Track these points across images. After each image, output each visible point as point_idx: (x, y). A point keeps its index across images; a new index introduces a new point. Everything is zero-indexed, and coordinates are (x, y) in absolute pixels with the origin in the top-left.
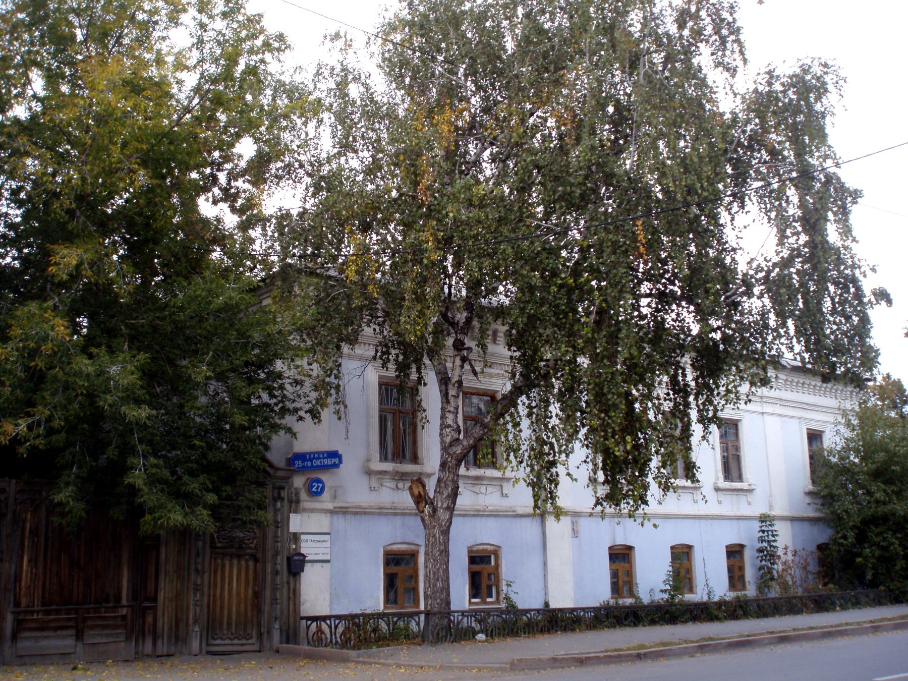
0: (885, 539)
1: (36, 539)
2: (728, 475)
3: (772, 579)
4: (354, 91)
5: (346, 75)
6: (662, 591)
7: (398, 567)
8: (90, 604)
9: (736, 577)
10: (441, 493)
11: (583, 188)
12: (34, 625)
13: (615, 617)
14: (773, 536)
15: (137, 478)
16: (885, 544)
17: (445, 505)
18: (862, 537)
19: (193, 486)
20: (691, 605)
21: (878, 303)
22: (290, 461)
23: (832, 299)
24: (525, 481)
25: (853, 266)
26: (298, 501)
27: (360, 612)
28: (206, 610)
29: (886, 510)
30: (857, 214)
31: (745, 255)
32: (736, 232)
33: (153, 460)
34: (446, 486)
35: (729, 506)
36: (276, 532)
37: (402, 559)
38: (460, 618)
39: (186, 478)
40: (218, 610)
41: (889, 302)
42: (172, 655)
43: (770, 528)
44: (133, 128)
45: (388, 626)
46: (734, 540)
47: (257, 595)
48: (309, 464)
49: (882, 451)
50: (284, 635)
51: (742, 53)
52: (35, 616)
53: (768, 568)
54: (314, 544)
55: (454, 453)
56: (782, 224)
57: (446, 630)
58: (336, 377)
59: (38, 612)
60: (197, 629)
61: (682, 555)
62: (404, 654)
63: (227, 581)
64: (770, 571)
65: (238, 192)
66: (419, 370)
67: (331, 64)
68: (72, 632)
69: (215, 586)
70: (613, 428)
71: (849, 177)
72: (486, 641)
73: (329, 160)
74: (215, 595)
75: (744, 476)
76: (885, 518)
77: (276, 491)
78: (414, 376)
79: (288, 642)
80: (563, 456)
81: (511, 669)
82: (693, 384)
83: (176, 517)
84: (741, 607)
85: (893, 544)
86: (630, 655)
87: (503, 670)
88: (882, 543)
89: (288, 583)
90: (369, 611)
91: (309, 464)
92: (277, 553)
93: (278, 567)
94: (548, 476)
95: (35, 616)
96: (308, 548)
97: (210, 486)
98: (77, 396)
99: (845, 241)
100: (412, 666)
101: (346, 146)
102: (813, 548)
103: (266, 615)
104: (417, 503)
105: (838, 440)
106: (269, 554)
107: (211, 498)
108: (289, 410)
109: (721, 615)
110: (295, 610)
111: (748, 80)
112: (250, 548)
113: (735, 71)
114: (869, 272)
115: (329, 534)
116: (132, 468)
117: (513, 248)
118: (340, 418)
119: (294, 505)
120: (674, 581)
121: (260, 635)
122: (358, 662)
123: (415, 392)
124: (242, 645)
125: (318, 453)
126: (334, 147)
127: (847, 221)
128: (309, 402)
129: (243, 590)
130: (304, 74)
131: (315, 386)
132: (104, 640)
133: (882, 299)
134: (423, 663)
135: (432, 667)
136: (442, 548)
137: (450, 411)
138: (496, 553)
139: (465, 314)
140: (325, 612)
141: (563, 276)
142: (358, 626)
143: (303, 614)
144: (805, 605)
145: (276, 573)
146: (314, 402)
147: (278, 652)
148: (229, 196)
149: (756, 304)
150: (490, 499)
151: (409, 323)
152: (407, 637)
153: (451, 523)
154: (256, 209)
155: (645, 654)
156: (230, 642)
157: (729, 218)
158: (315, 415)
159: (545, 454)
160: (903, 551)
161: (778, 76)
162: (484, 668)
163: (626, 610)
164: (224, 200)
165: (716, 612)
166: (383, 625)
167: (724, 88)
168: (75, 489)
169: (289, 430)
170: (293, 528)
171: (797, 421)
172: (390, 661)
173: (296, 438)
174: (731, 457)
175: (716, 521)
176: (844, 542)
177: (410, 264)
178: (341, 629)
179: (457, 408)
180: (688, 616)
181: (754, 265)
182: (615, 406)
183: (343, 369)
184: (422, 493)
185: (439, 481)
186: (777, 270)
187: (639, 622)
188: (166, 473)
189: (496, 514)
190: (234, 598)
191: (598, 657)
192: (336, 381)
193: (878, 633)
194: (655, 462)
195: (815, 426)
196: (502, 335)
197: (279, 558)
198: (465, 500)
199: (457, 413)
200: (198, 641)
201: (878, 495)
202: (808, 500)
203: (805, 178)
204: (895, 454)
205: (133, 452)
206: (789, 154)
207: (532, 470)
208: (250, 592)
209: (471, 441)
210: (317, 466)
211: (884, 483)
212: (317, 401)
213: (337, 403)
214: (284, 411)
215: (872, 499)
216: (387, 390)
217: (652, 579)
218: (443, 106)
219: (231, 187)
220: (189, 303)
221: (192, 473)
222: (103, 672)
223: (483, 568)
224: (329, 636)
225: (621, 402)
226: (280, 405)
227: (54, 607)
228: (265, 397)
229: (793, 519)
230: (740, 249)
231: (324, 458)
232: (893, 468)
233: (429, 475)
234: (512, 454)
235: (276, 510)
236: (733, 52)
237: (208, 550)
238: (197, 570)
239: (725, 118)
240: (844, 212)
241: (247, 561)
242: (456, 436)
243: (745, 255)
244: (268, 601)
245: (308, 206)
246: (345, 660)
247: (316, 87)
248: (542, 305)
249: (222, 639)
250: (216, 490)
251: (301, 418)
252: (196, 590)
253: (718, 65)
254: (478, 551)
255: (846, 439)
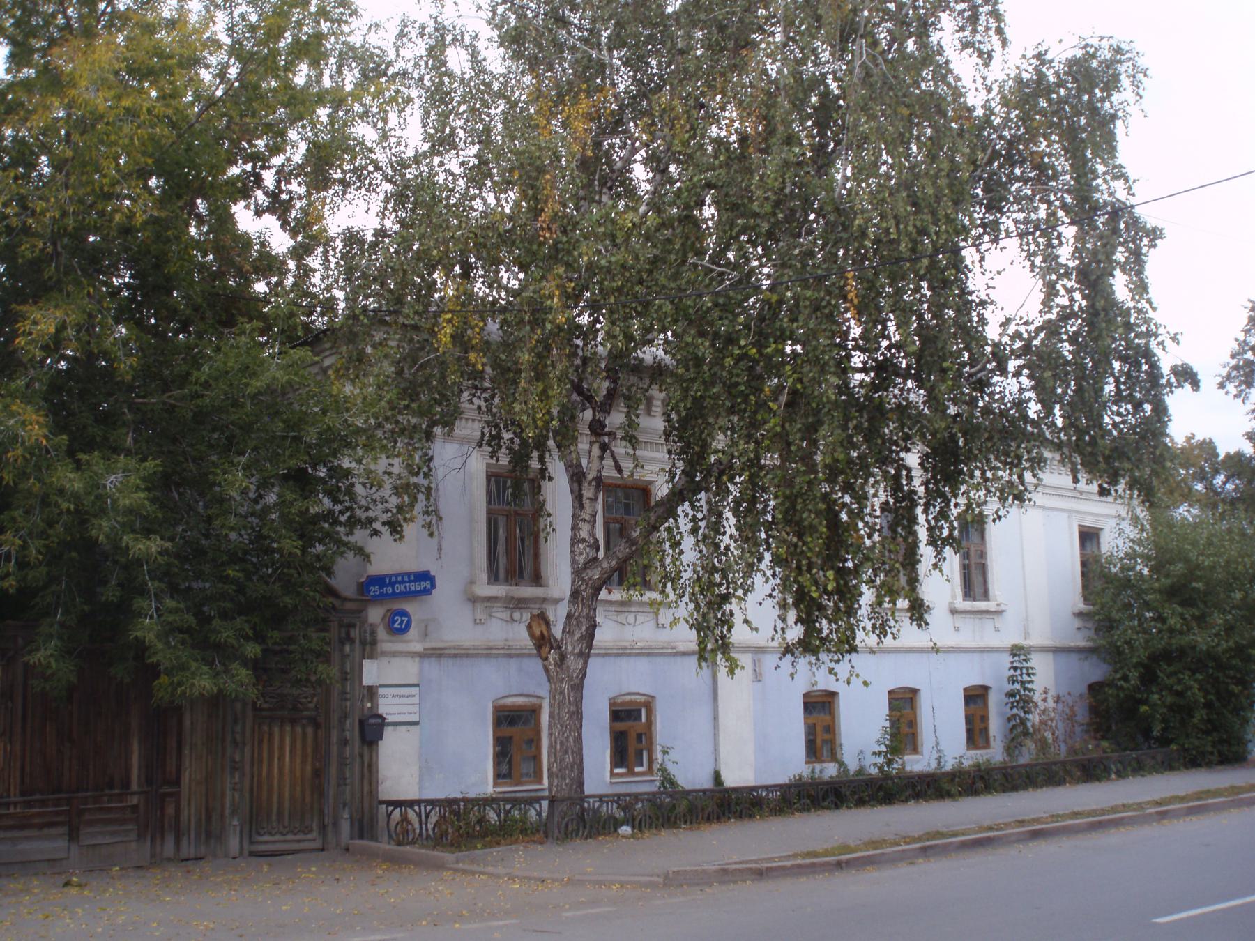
0: (1180, 681)
1: (10, 704)
2: (968, 592)
3: (1026, 734)
4: (457, 60)
5: (442, 36)
6: (875, 753)
7: (513, 728)
8: (87, 790)
9: (976, 733)
10: (571, 633)
11: (772, 220)
12: (11, 822)
13: (809, 796)
14: (1028, 675)
15: (147, 628)
16: (1179, 688)
17: (577, 650)
18: (1149, 677)
19: (225, 633)
20: (913, 777)
21: (1179, 386)
22: (363, 588)
23: (1117, 382)
24: (687, 622)
25: (1149, 334)
26: (374, 643)
27: (460, 796)
28: (247, 795)
29: (1183, 643)
30: (1156, 263)
31: (998, 312)
32: (986, 279)
33: (170, 603)
34: (578, 624)
35: (969, 634)
36: (344, 686)
37: (520, 717)
38: (597, 805)
39: (216, 623)
40: (265, 794)
41: (1195, 384)
42: (201, 858)
43: (1025, 664)
44: (132, 139)
45: (499, 815)
46: (976, 680)
47: (317, 774)
48: (390, 590)
49: (1180, 560)
50: (357, 825)
51: (999, 31)
52: (12, 810)
53: (1020, 718)
54: (397, 700)
55: (590, 579)
56: (1050, 267)
57: (580, 820)
58: (426, 476)
59: (15, 804)
60: (235, 822)
61: (903, 703)
62: (520, 860)
63: (276, 755)
64: (1023, 722)
65: (291, 199)
66: (542, 459)
67: (421, 21)
68: (63, 830)
69: (261, 761)
70: (809, 558)
71: (1149, 215)
72: (633, 836)
73: (416, 160)
74: (260, 775)
75: (991, 593)
76: (1182, 652)
77: (343, 631)
78: (535, 464)
79: (361, 837)
80: (740, 592)
81: (665, 884)
82: (921, 490)
83: (203, 683)
84: (982, 778)
85: (1191, 688)
86: (827, 864)
87: (653, 885)
88: (1175, 687)
89: (361, 756)
90: (471, 795)
91: (390, 590)
92: (344, 716)
93: (348, 734)
94: (719, 615)
95: (12, 810)
96: (389, 706)
97: (251, 633)
98: (61, 514)
99: (1138, 302)
100: (530, 879)
101: (442, 142)
102: (1083, 689)
103: (331, 801)
104: (539, 647)
105: (1121, 545)
106: (335, 717)
107: (252, 650)
108: (359, 520)
109: (953, 790)
110: (371, 792)
111: (1010, 63)
112: (307, 709)
113: (990, 57)
114: (1168, 343)
115: (417, 685)
116: (140, 615)
117: (672, 303)
118: (431, 535)
119: (370, 648)
120: (891, 741)
121: (323, 828)
122: (456, 870)
123: (536, 490)
124: (299, 841)
125: (403, 575)
126: (424, 140)
127: (1139, 273)
128: (387, 511)
129: (298, 767)
130: (381, 32)
131: (396, 488)
132: (108, 840)
133: (1185, 381)
134: (545, 875)
135: (557, 880)
136: (572, 708)
137: (584, 520)
138: (649, 704)
139: (606, 384)
140: (411, 793)
141: (743, 343)
142: (457, 814)
143: (382, 797)
144: (1068, 772)
145: (344, 742)
146: (395, 511)
147: (347, 850)
148: (278, 206)
149: (1011, 386)
150: (641, 630)
151: (525, 412)
152: (524, 831)
153: (585, 675)
154: (316, 229)
155: (848, 862)
156: (282, 838)
157: (977, 257)
158: (395, 528)
159: (715, 585)
160: (1205, 697)
161: (1051, 61)
162: (628, 883)
163: (825, 787)
164: (271, 210)
165: (946, 787)
166: (492, 816)
167: (974, 81)
168: (59, 644)
169: (360, 551)
170: (367, 680)
171: (1066, 515)
172: (500, 870)
173: (369, 561)
174: (973, 566)
175: (952, 656)
176: (1125, 685)
177: (528, 328)
178: (434, 818)
179: (594, 516)
180: (909, 792)
181: (1012, 329)
182: (813, 528)
183: (437, 462)
184: (545, 633)
185: (569, 616)
186: (1042, 335)
187: (842, 803)
188: (191, 620)
189: (649, 653)
190: (287, 778)
191: (783, 868)
192: (426, 483)
193: (1165, 822)
194: (867, 596)
195: (1090, 522)
196: (659, 403)
197: (348, 722)
198: (604, 635)
199: (594, 522)
200: (238, 839)
201: (1172, 622)
202: (1077, 623)
203: (1084, 208)
204: (1198, 567)
205: (143, 592)
206: (1062, 164)
207: (697, 608)
208: (309, 768)
209: (614, 563)
210: (401, 593)
211: (1182, 604)
212: (400, 508)
213: (427, 513)
214: (353, 523)
215: (1165, 627)
216: (497, 483)
217: (862, 734)
218: (577, 94)
219: (282, 191)
220: (216, 379)
221: (224, 615)
222: (105, 891)
223: (631, 729)
224: (417, 826)
225: (820, 523)
226: (348, 514)
227: (38, 797)
228: (327, 502)
229: (1056, 650)
230: (992, 303)
231: (410, 581)
232: (1194, 584)
233: (557, 601)
234: (669, 584)
235: (344, 657)
236: (987, 29)
237: (250, 713)
238: (234, 742)
239: (975, 114)
240: (1136, 263)
241: (304, 727)
242: (592, 554)
243: (998, 312)
244: (333, 782)
245: (388, 224)
246: (440, 866)
247: (398, 55)
248: (713, 384)
249: (270, 834)
250: (259, 638)
251: (376, 533)
252: (234, 769)
253: (966, 45)
254: (623, 703)
255: (1132, 540)
